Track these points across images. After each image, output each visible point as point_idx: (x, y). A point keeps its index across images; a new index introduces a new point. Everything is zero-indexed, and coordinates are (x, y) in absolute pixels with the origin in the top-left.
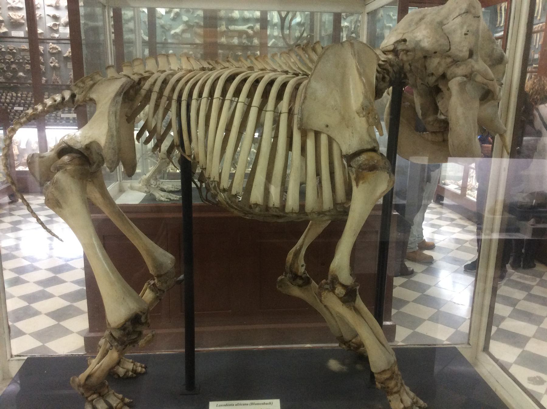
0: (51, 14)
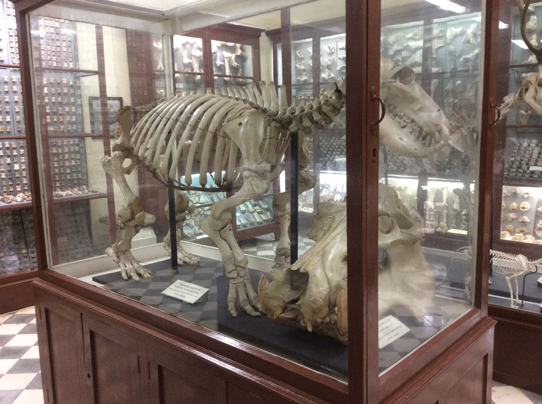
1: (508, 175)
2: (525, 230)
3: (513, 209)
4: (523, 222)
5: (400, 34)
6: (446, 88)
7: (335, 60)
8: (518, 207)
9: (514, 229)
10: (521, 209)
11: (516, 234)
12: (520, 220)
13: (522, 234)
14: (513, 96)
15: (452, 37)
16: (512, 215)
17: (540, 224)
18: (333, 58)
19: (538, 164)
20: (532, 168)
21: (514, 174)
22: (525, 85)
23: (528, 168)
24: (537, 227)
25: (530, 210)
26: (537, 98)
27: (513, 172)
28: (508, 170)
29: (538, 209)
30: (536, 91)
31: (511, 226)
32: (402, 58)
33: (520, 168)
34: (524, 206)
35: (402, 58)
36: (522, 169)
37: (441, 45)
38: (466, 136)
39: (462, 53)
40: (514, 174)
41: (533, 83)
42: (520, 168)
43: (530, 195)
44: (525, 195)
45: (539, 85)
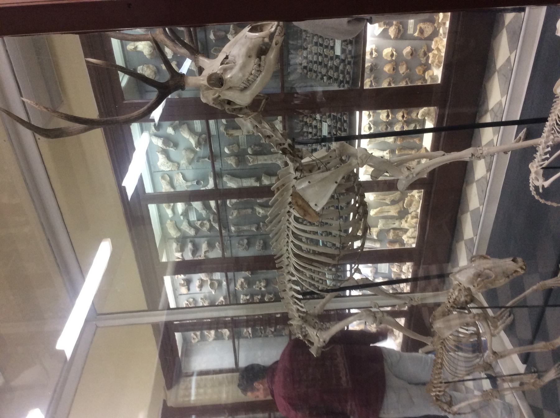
0: (198, 290)
1: (348, 82)
2: (423, 50)
3: (394, 70)
4: (412, 55)
5: (169, 225)
6: (234, 166)
7: (202, 296)
8: (390, 62)
9: (421, 65)
10: (394, 58)
11: (430, 62)
12: (409, 58)
13: (431, 55)
14: (241, 119)
15: (170, 163)
16: (402, 70)
17: (415, 32)
18: (200, 300)
19: (332, 45)
20: (338, 51)
21: (347, 76)
22: (222, 106)
23: (337, 57)
24: (419, 36)
25: (393, 47)
26: (243, 86)
27: (344, 77)
28: (341, 83)
29: (392, 37)
30: (230, 88)
31: (417, 70)
32: (198, 220)
33: (337, 68)
34: (389, 55)
35: (198, 220)
36: (340, 65)
37: (181, 176)
38: (309, 182)
39: (190, 149)
40: (347, 76)
41: (217, 95)
42: (337, 68)
43: (374, 48)
44: (374, 56)
45: (222, 85)
